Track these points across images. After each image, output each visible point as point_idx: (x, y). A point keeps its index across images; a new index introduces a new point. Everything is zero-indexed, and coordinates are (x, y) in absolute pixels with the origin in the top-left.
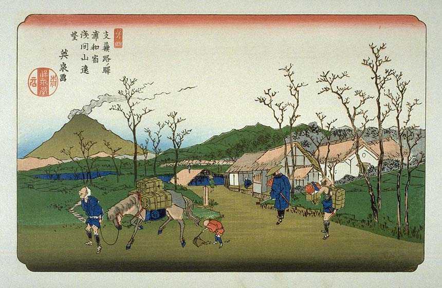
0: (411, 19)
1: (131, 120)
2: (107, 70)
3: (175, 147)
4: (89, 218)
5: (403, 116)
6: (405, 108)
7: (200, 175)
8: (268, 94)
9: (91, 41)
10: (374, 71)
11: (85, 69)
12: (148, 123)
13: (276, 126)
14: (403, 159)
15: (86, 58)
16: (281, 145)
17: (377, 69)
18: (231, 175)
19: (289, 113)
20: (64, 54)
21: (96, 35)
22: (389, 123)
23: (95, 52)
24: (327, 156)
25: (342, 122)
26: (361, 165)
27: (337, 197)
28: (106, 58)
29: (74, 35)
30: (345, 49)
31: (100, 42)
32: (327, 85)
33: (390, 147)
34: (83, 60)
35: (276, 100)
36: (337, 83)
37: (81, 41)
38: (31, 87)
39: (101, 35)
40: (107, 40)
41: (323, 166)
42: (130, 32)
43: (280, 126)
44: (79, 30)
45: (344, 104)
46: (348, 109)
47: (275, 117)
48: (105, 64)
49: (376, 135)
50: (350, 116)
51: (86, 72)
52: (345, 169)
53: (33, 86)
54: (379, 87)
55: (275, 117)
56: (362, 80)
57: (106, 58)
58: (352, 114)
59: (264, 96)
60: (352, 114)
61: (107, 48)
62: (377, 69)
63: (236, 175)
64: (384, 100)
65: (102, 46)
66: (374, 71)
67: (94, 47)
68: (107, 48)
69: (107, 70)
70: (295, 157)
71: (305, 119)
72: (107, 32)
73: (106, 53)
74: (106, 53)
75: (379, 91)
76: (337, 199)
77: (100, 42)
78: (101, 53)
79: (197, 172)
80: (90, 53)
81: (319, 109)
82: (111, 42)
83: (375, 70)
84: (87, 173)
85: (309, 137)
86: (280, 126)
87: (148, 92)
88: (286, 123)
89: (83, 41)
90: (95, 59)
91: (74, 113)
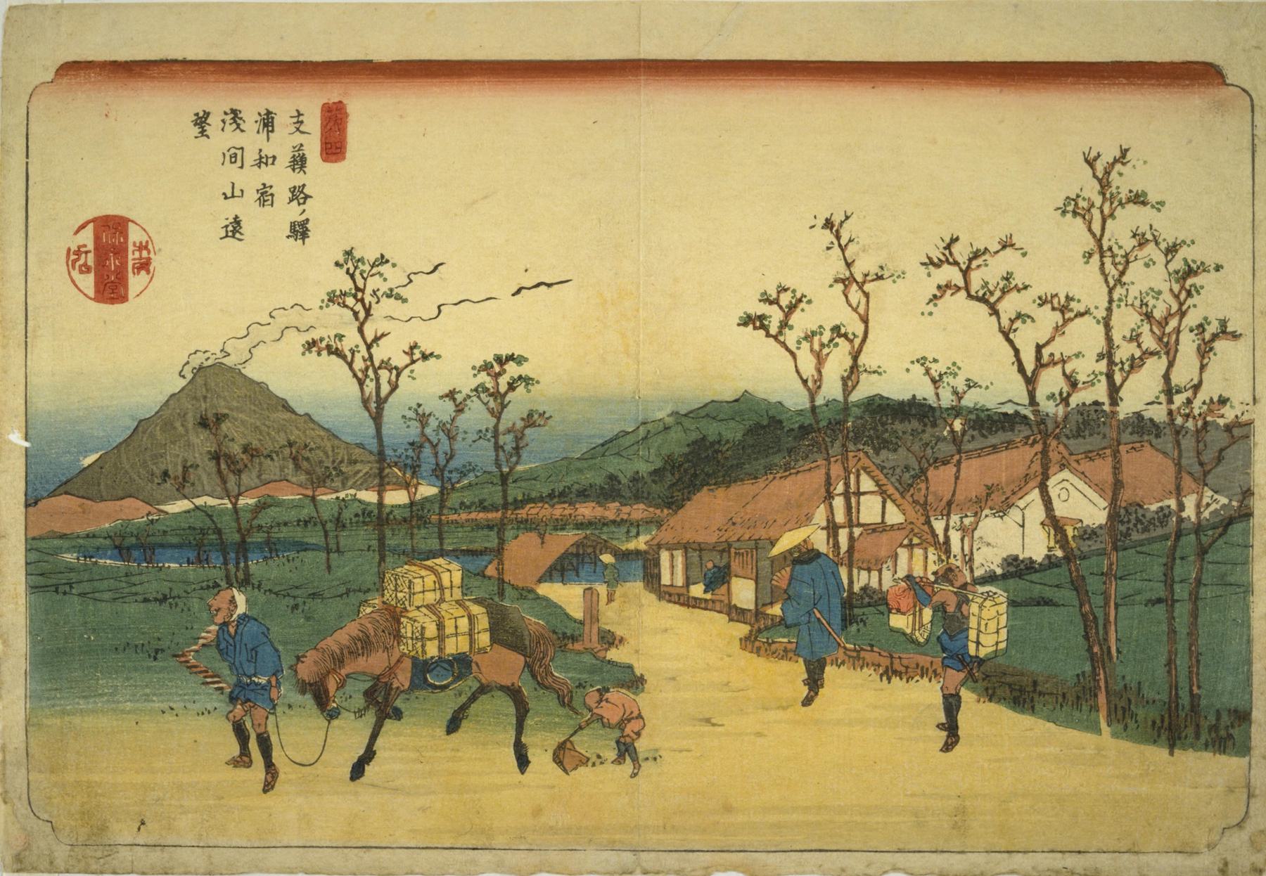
0: (1200, 74)
1: (370, 386)
2: (300, 231)
3: (499, 466)
4: (239, 681)
5: (1184, 372)
6: (1188, 345)
7: (574, 550)
8: (778, 303)
9: (251, 140)
10: (1094, 235)
11: (235, 228)
12: (423, 387)
13: (796, 399)
14: (1181, 507)
15: (237, 193)
16: (97, 291)
17: (1103, 229)
18: (665, 556)
19: (838, 362)
20: (385, 280)
21: (268, 122)
22: (1140, 393)
23: (267, 175)
24: (953, 495)
25: (1000, 388)
26: (1054, 523)
27: (983, 623)
28: (299, 195)
29: (201, 121)
30: (1003, 173)
31: (282, 143)
32: (951, 274)
33: (1147, 471)
34: (226, 198)
35: (802, 321)
36: (987, 274)
37: (222, 138)
38: (75, 274)
39: (283, 121)
40: (299, 139)
41: (939, 526)
42: (368, 110)
43: (812, 400)
44: (216, 100)
45: (1006, 335)
46: (1017, 352)
47: (797, 371)
48: (293, 213)
49: (1087, 432)
50: (1021, 370)
51: (238, 235)
52: (1014, 535)
53: (81, 272)
54: (1112, 283)
55: (797, 371)
56: (1056, 260)
57: (299, 195)
58: (1029, 367)
59: (764, 309)
60: (1029, 367)
61: (299, 162)
62: (1103, 229)
63: (679, 555)
64: (1125, 320)
65: (284, 159)
66: (1094, 235)
67: (262, 161)
68: (299, 162)
69: (300, 231)
70: (853, 500)
71: (896, 380)
72: (299, 114)
73: (297, 179)
74: (297, 179)
75: (1111, 291)
76: (982, 628)
77: (282, 143)
78: (281, 178)
79: (569, 538)
80: (250, 179)
81: (921, 346)
82: (313, 148)
83: (1096, 227)
84: (225, 547)
85: (896, 433)
86: (812, 400)
87: (423, 296)
88: (832, 389)
89: (231, 138)
90: (265, 196)
91: (196, 361)
